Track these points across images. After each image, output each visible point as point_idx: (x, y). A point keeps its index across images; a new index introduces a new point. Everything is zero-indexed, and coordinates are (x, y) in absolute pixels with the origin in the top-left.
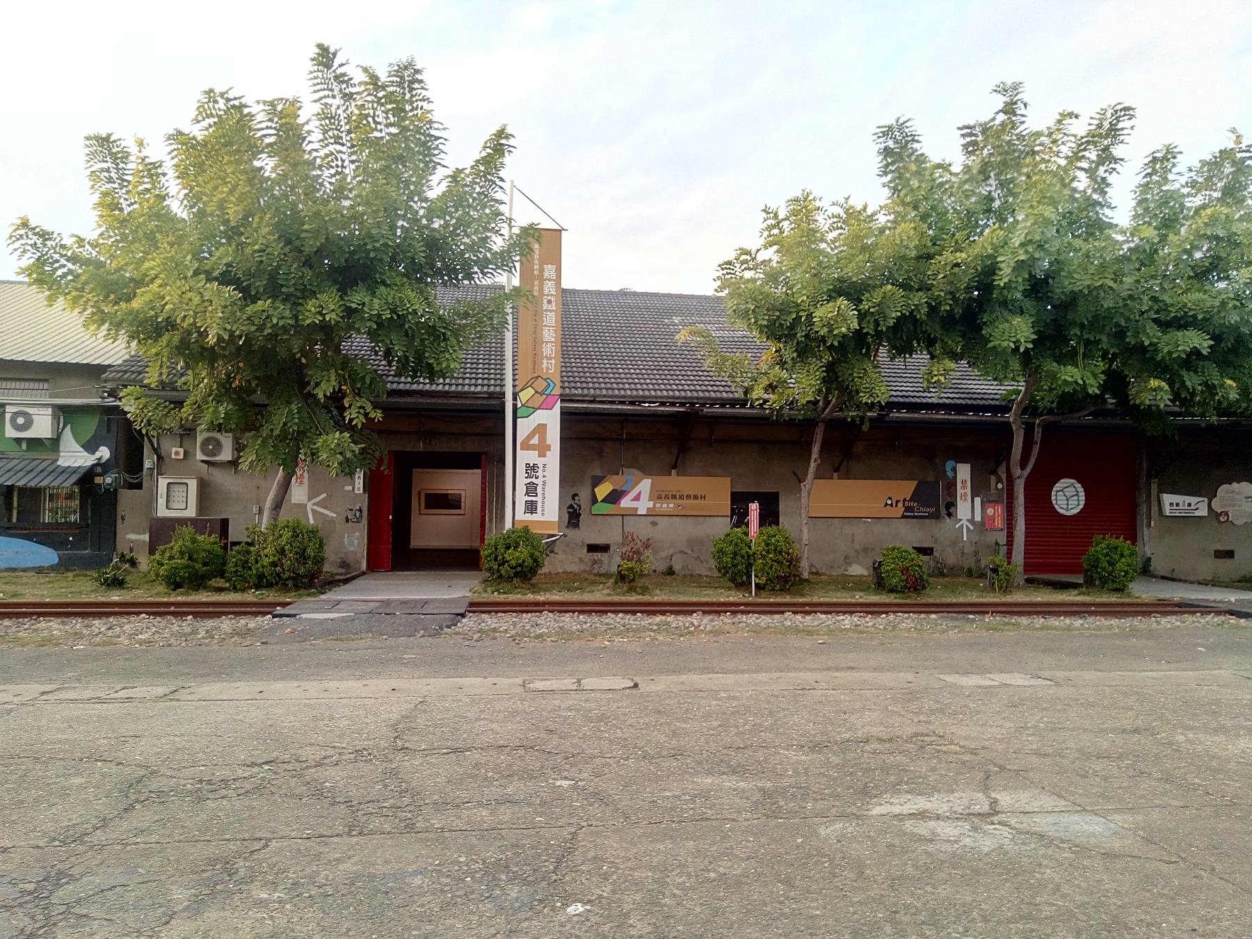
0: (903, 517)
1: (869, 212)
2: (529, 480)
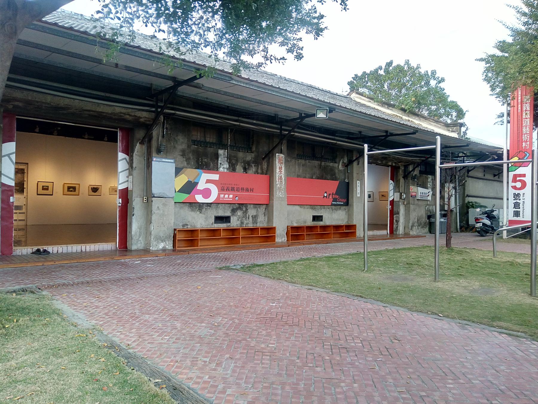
0: (332, 205)
1: (496, 96)
2: (515, 201)
